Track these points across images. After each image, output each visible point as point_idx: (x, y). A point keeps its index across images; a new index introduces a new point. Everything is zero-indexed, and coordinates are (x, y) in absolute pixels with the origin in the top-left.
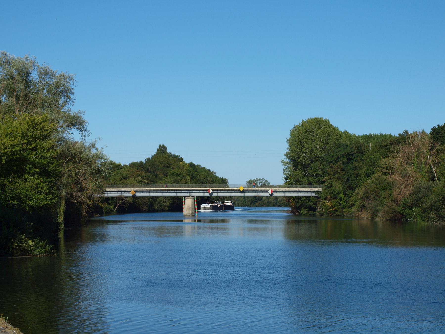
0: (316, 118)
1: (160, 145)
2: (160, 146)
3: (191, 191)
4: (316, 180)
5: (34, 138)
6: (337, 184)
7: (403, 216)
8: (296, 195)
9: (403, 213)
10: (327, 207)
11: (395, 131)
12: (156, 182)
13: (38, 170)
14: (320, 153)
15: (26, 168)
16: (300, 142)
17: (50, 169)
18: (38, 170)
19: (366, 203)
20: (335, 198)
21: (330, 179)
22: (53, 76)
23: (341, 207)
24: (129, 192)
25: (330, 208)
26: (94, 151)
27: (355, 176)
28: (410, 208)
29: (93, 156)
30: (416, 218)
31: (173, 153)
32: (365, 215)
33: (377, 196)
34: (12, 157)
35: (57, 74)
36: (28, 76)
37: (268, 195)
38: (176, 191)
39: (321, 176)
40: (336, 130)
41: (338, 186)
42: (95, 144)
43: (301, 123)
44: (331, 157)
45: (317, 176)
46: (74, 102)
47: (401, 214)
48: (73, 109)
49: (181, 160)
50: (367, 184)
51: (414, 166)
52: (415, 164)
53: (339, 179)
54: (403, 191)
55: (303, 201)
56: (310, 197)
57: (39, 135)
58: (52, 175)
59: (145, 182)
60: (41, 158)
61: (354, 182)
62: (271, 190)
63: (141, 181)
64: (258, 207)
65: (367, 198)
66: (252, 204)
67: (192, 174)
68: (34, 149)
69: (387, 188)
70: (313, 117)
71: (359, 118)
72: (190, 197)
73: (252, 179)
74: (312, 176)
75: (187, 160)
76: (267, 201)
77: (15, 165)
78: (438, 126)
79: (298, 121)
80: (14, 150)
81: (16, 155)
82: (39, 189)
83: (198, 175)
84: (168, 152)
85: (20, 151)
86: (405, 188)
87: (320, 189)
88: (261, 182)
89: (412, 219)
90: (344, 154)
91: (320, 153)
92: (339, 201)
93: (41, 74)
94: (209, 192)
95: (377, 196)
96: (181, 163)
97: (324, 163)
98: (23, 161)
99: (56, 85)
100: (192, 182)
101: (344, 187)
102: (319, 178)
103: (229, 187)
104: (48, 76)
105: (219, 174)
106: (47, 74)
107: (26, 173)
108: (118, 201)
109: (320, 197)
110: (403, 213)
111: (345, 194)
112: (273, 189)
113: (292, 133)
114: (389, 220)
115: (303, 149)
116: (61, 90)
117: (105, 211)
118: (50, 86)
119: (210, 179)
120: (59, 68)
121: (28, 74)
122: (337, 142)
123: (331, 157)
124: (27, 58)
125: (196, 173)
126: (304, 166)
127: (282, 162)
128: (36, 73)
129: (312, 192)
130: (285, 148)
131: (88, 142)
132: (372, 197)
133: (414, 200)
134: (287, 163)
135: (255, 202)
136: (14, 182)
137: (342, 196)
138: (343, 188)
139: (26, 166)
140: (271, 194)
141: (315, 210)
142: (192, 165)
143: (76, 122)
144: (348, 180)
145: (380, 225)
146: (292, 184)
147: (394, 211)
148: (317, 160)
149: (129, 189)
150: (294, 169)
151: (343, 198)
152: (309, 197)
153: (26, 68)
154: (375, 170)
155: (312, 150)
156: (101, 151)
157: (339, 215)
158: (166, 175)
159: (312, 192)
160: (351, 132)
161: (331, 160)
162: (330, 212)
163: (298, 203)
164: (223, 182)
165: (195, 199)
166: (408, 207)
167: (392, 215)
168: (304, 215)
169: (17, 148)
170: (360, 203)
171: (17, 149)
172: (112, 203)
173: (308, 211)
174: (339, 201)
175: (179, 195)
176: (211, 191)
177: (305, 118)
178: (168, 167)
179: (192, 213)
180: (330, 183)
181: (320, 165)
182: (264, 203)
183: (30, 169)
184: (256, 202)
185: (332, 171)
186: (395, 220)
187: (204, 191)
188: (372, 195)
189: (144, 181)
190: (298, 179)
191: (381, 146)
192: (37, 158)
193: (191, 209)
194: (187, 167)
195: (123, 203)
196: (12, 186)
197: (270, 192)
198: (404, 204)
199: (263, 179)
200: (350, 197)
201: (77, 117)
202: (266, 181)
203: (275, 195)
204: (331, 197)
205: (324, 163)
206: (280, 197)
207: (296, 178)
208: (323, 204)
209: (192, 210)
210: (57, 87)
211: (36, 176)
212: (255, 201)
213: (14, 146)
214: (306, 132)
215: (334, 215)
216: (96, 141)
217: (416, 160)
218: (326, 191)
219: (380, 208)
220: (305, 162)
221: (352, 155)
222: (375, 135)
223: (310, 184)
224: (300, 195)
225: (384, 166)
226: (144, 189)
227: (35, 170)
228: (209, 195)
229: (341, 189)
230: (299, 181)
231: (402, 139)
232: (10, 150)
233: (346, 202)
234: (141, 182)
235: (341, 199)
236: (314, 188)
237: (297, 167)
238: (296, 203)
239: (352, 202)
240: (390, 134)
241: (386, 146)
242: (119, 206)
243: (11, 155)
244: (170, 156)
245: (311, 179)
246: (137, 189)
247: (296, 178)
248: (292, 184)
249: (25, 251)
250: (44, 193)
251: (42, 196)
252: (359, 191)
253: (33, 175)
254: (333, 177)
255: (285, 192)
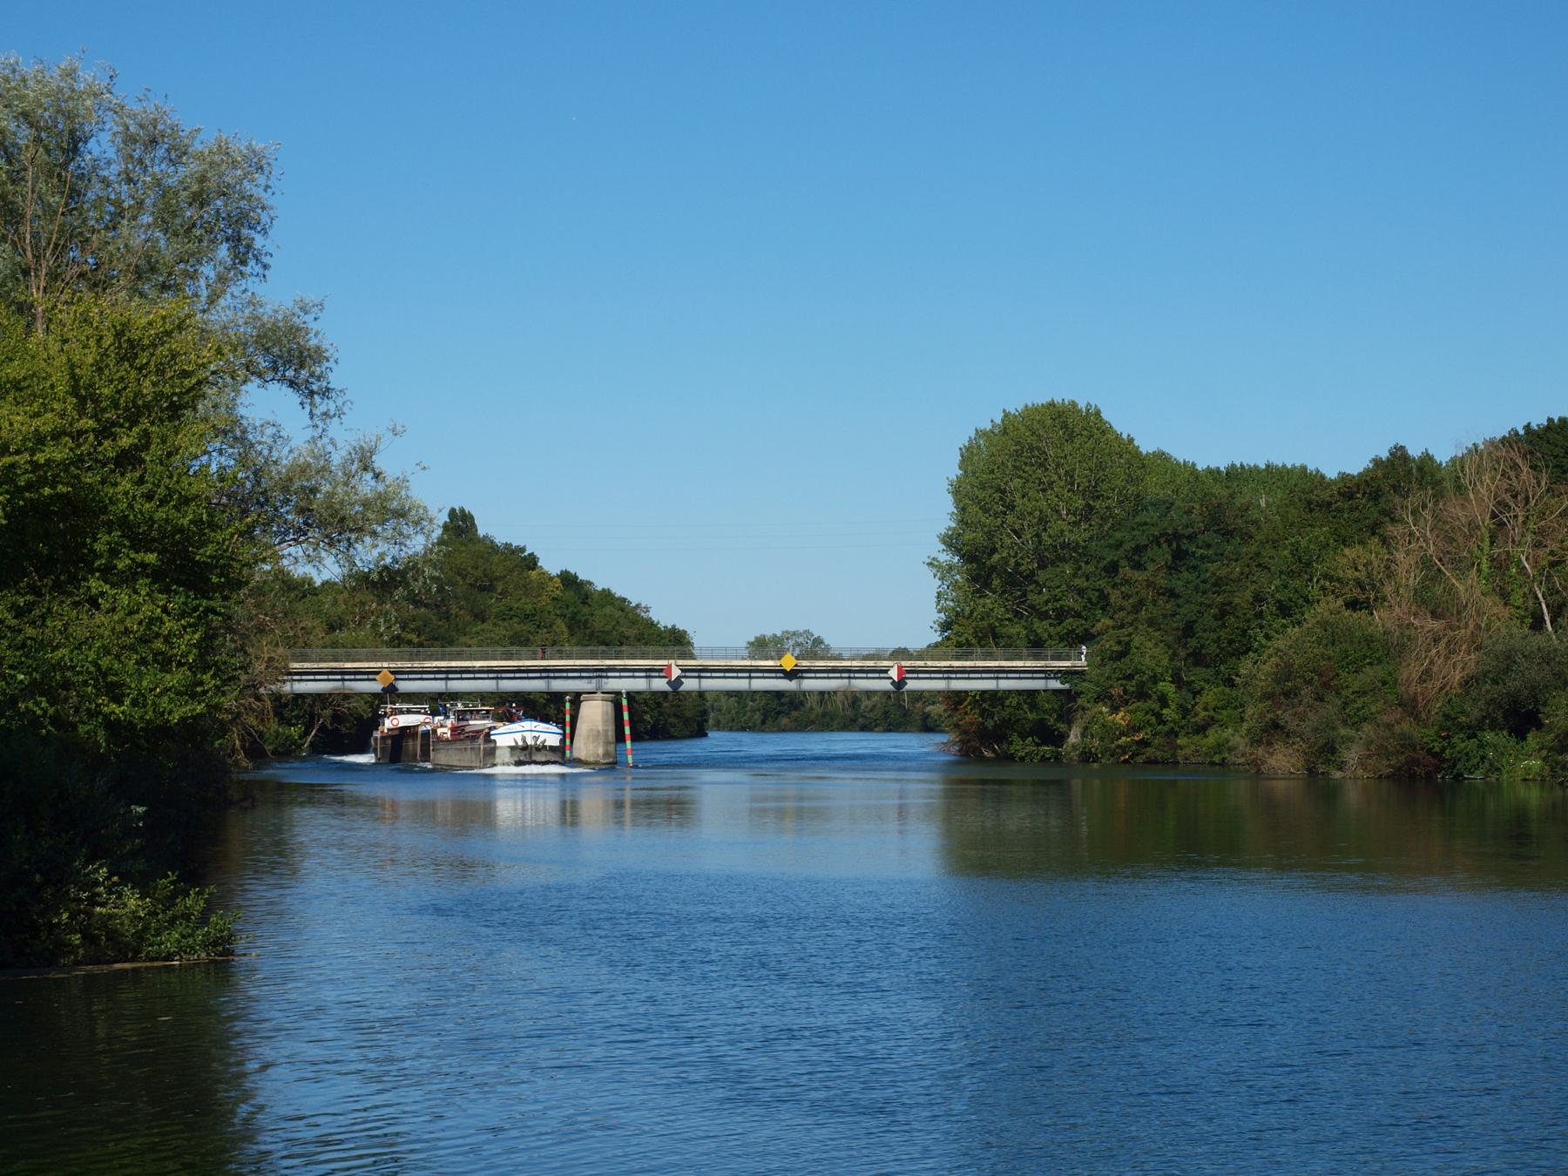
0: (1052, 404)
1: (453, 511)
2: (452, 513)
3: (601, 672)
4: (1059, 629)
5: (126, 409)
6: (1150, 645)
7: (1444, 761)
8: (989, 685)
9: (1443, 750)
10: (1110, 732)
11: (1341, 454)
12: (451, 643)
13: (151, 558)
14: (1062, 529)
15: (97, 547)
16: (999, 490)
17: (210, 550)
18: (151, 558)
19: (1286, 716)
20: (1142, 695)
21: (1122, 626)
22: (178, 154)
23: (1166, 728)
24: (371, 674)
25: (1123, 734)
26: (367, 486)
27: (1215, 617)
28: (1472, 732)
29: (366, 504)
30: (1498, 769)
31: (500, 539)
32: (1283, 760)
33: (1327, 685)
34: (34, 496)
35: (198, 146)
36: (75, 150)
37: (886, 685)
38: (546, 673)
39: (1078, 615)
40: (1126, 448)
41: (1151, 652)
42: (372, 453)
43: (998, 421)
44: (1110, 546)
45: (1061, 615)
46: (265, 267)
47: (1435, 755)
48: (274, 291)
49: (531, 562)
50: (1286, 643)
51: (1479, 571)
52: (1484, 566)
53: (1151, 622)
54: (1442, 668)
55: (1008, 710)
56: (1038, 691)
57: (155, 392)
58: (215, 580)
59: (410, 643)
60: (163, 502)
61: (1213, 636)
62: (900, 668)
63: (398, 637)
64: (791, 730)
65: (1286, 695)
66: (769, 722)
67: (574, 615)
68: (127, 459)
69: (1365, 657)
70: (1042, 399)
71: (1252, 388)
72: (599, 695)
73: (768, 633)
74: (1044, 616)
75: (551, 564)
76: (820, 711)
77: (34, 536)
78: (1527, 427)
79: (988, 416)
80: (40, 458)
81: (53, 487)
82: (159, 645)
83: (590, 618)
84: (481, 532)
85: (65, 466)
86: (1447, 658)
87: (1082, 663)
88: (799, 644)
89: (1478, 775)
90: (1162, 535)
91: (1062, 529)
92: (1156, 706)
93: (130, 139)
94: (668, 675)
95: (1327, 685)
96: (533, 574)
97: (1090, 568)
98: (83, 511)
99: (195, 187)
100: (574, 640)
101: (1175, 654)
102: (1069, 623)
103: (692, 657)
104: (161, 152)
105: (663, 617)
106: (153, 142)
107: (92, 572)
108: (317, 709)
109: (1079, 694)
110: (1443, 750)
111: (1177, 680)
112: (904, 663)
113: (968, 456)
114: (1388, 777)
115: (1010, 518)
116: (216, 215)
117: (269, 748)
118: (166, 193)
119: (631, 633)
120: (208, 117)
121: (74, 144)
122: (1132, 489)
123: (1110, 546)
124: (70, 74)
125: (586, 610)
126: (1017, 582)
127: (930, 564)
128: (105, 137)
129: (1048, 674)
130: (941, 514)
131: (342, 439)
132: (1306, 691)
133: (1488, 703)
134: (951, 568)
135: (779, 713)
136: (37, 612)
137: (1167, 687)
138: (1171, 660)
139: (95, 540)
140: (899, 684)
141: (1060, 739)
142: (568, 580)
143: (291, 357)
144: (1188, 630)
145: (1352, 796)
146: (969, 644)
147: (1407, 744)
148: (1063, 560)
149: (372, 664)
150: (978, 591)
151: (1171, 695)
152: (1032, 694)
153: (70, 116)
154: (1314, 591)
155: (1043, 520)
156: (402, 482)
157: (1155, 762)
158: (480, 617)
159: (1048, 674)
160: (1182, 453)
161: (1110, 556)
162: (1124, 749)
163: (992, 716)
164: (676, 641)
165: (625, 702)
166: (1461, 728)
167: (1402, 758)
168: (1022, 759)
169: (58, 453)
170: (1262, 715)
171: (58, 456)
172: (297, 717)
173: (1038, 745)
174: (1156, 706)
175: (558, 685)
176: (676, 673)
177: (1015, 406)
178: (486, 586)
179: (606, 754)
180: (1119, 643)
181: (1075, 575)
182: (813, 717)
183: (114, 553)
184: (780, 712)
185: (1126, 597)
186: (1413, 777)
187: (649, 672)
188: (1309, 682)
189: (409, 636)
190: (993, 629)
191: (1310, 503)
192: (149, 497)
193: (602, 740)
194: (556, 589)
195: (337, 718)
196: (30, 631)
197: (894, 674)
198: (1447, 717)
199: (806, 632)
200: (1199, 692)
201: (294, 331)
202: (818, 641)
203: (912, 685)
204: (1125, 691)
205: (1090, 568)
206: (869, 694)
207: (985, 623)
208: (1093, 720)
209: (607, 743)
210: (200, 200)
211: (143, 585)
212: (789, 708)
213: (40, 440)
214: (1019, 454)
215: (1140, 759)
216: (379, 438)
217: (1486, 549)
218: (1107, 670)
219: (1343, 731)
220: (1018, 564)
221: (1191, 538)
222: (1251, 470)
223: (1036, 646)
224: (1005, 685)
225: (1350, 574)
226: (428, 664)
227: (139, 557)
228: (667, 688)
229: (1165, 662)
230: (995, 636)
231: (1385, 476)
232: (27, 456)
233: (1185, 711)
234: (397, 641)
235: (1163, 701)
236: (1053, 659)
237: (987, 584)
238: (982, 715)
239: (1206, 709)
240: (1304, 468)
241: (1329, 504)
242: (322, 728)
243: (30, 486)
244: (490, 547)
245: (1041, 627)
246: (399, 664)
247: (985, 623)
248: (969, 644)
249: (108, 943)
250: (180, 664)
251: (175, 678)
252: (1257, 670)
253: (128, 579)
254: (1130, 618)
255: (948, 673)
